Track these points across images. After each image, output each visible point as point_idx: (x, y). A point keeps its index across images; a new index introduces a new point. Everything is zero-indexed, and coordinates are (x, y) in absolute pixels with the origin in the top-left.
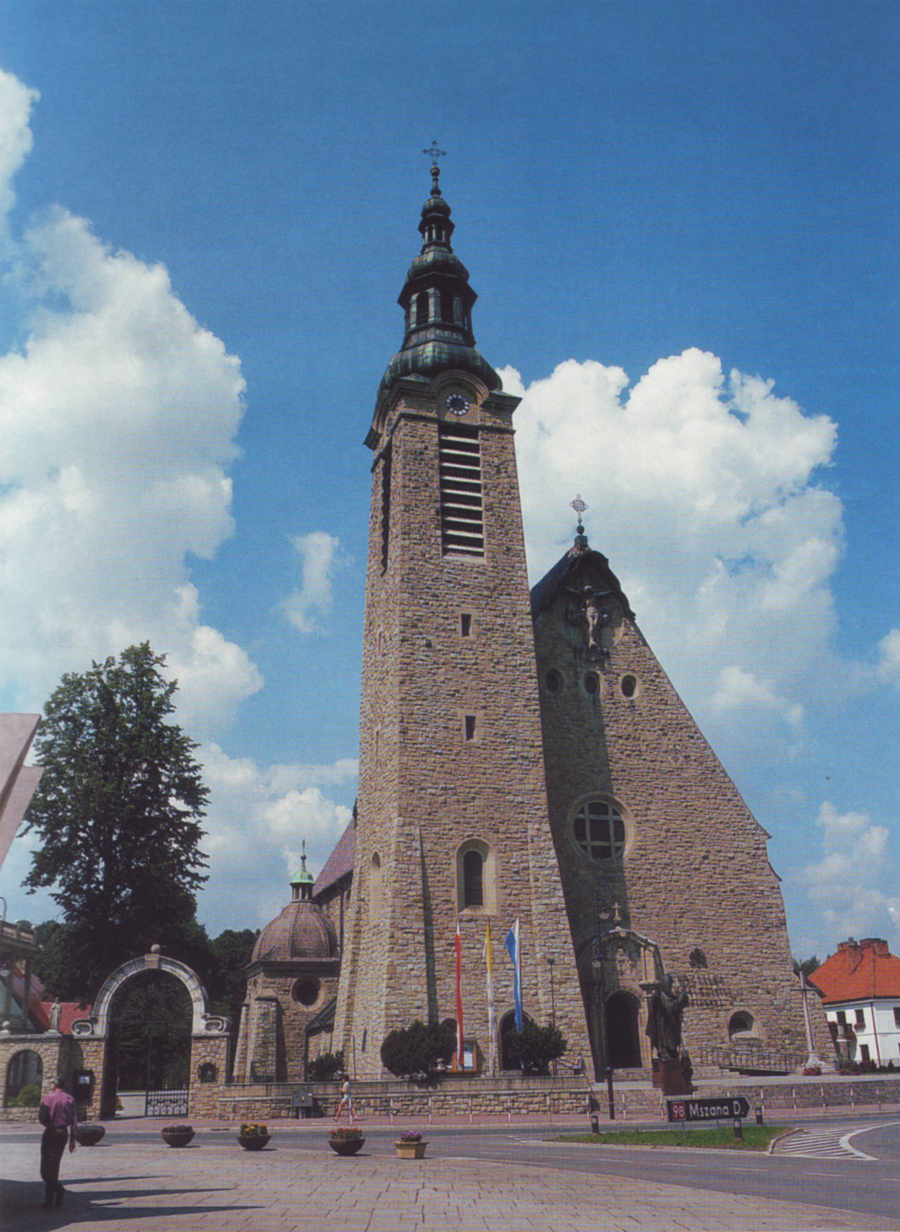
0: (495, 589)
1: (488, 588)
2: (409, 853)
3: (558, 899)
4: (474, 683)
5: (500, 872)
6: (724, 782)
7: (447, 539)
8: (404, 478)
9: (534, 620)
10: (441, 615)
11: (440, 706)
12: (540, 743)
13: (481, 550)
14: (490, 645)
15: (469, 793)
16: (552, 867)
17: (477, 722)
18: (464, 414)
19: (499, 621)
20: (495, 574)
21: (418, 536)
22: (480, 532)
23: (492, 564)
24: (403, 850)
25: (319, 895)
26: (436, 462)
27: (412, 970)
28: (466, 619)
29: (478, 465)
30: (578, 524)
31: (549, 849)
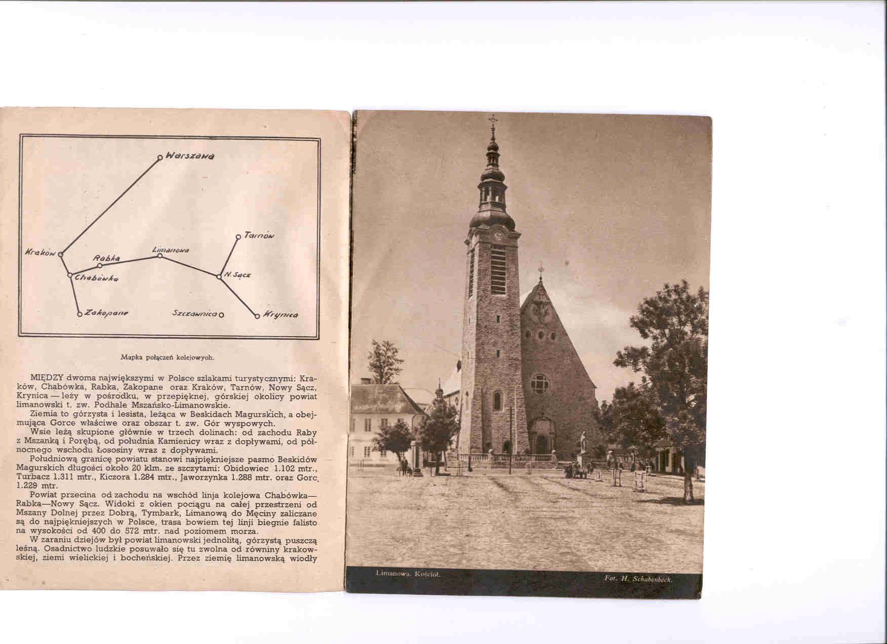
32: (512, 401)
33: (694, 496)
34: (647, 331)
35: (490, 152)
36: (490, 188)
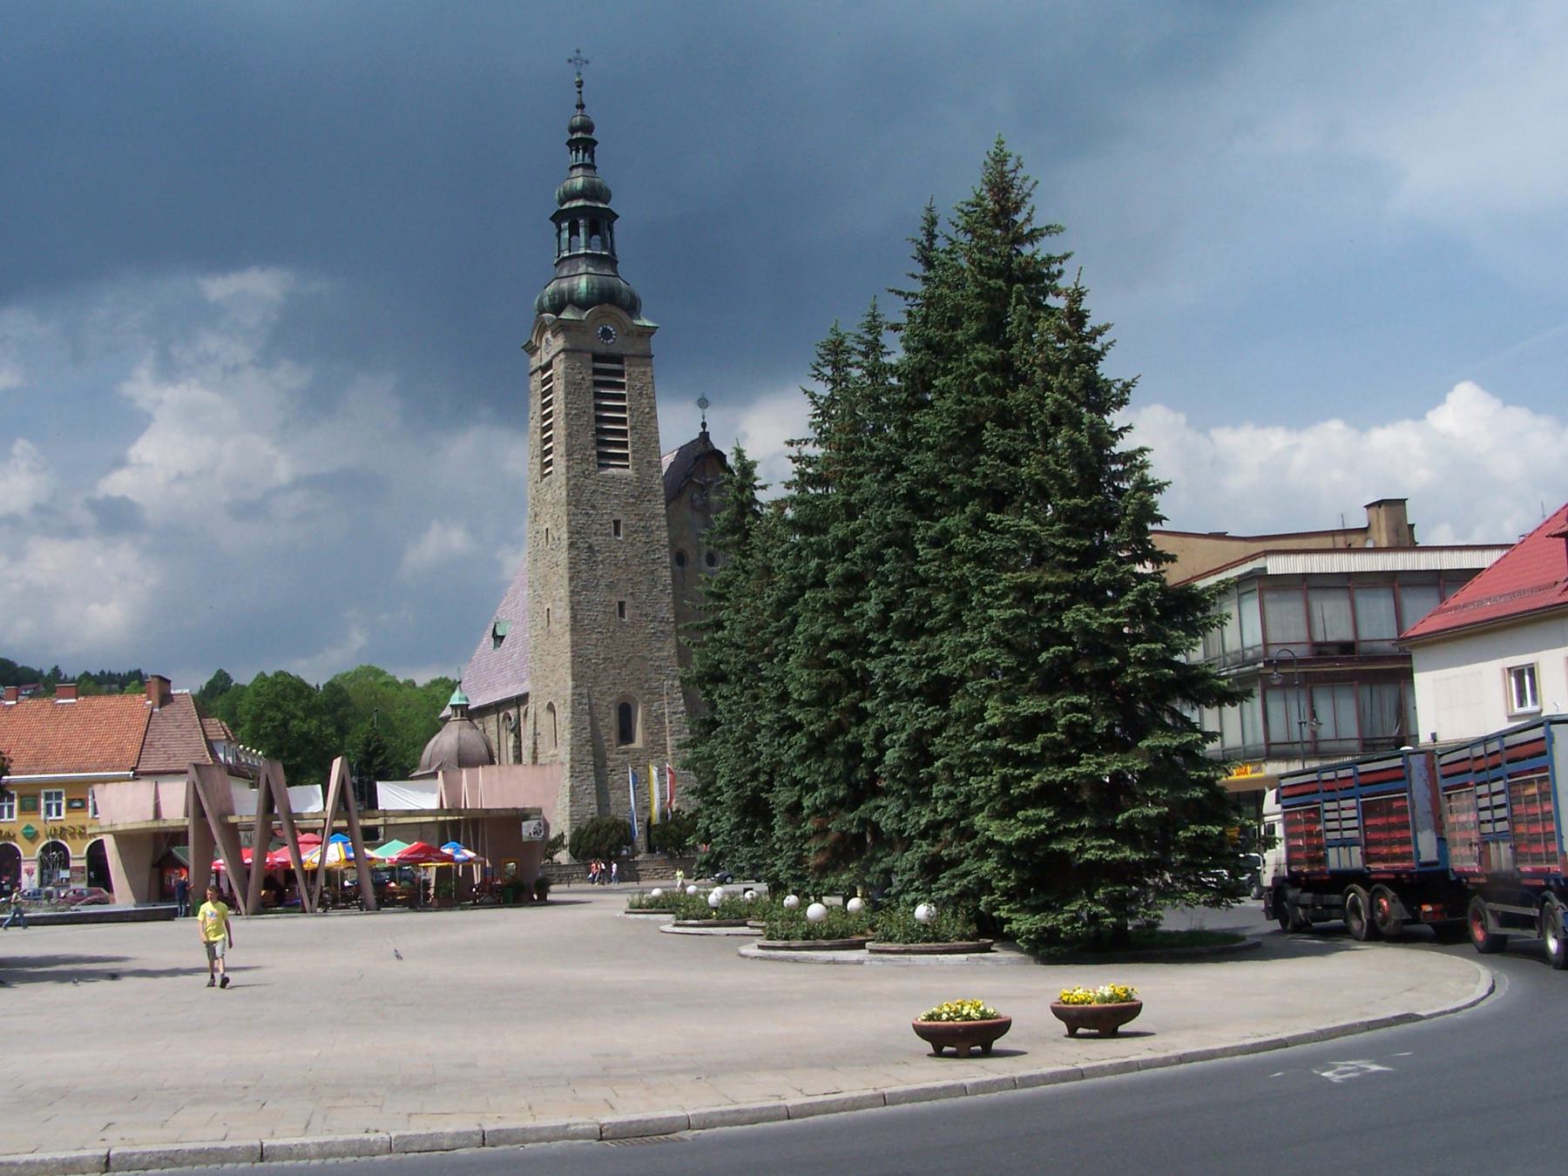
1: (632, 496)
5: (646, 717)
7: (601, 455)
8: (566, 407)
9: (666, 508)
12: (683, 708)
16: (682, 712)
19: (642, 524)
22: (626, 448)
26: (592, 411)
28: (617, 523)
29: (624, 401)
32: (659, 719)
33: (1391, 603)
34: (1026, 230)
35: (574, 137)
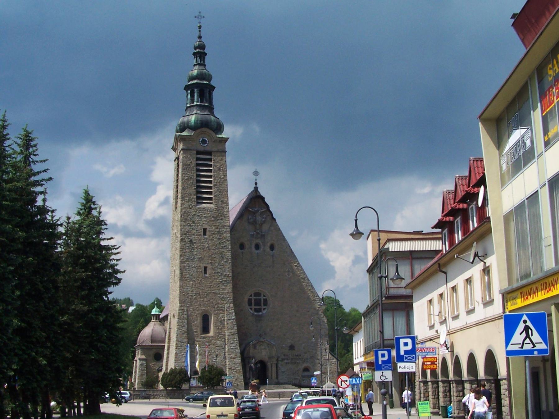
0: (216, 217)
1: (213, 217)
2: (183, 316)
3: (235, 330)
4: (207, 255)
6: (308, 283)
10: (195, 229)
11: (195, 263)
13: (212, 202)
14: (213, 240)
15: (205, 294)
16: (233, 319)
17: (208, 269)
18: (206, 146)
19: (217, 230)
20: (216, 211)
21: (187, 199)
23: (215, 207)
24: (181, 315)
25: (162, 318)
27: (183, 355)
28: (205, 230)
30: (255, 182)
31: (233, 313)
36: (196, 90)
